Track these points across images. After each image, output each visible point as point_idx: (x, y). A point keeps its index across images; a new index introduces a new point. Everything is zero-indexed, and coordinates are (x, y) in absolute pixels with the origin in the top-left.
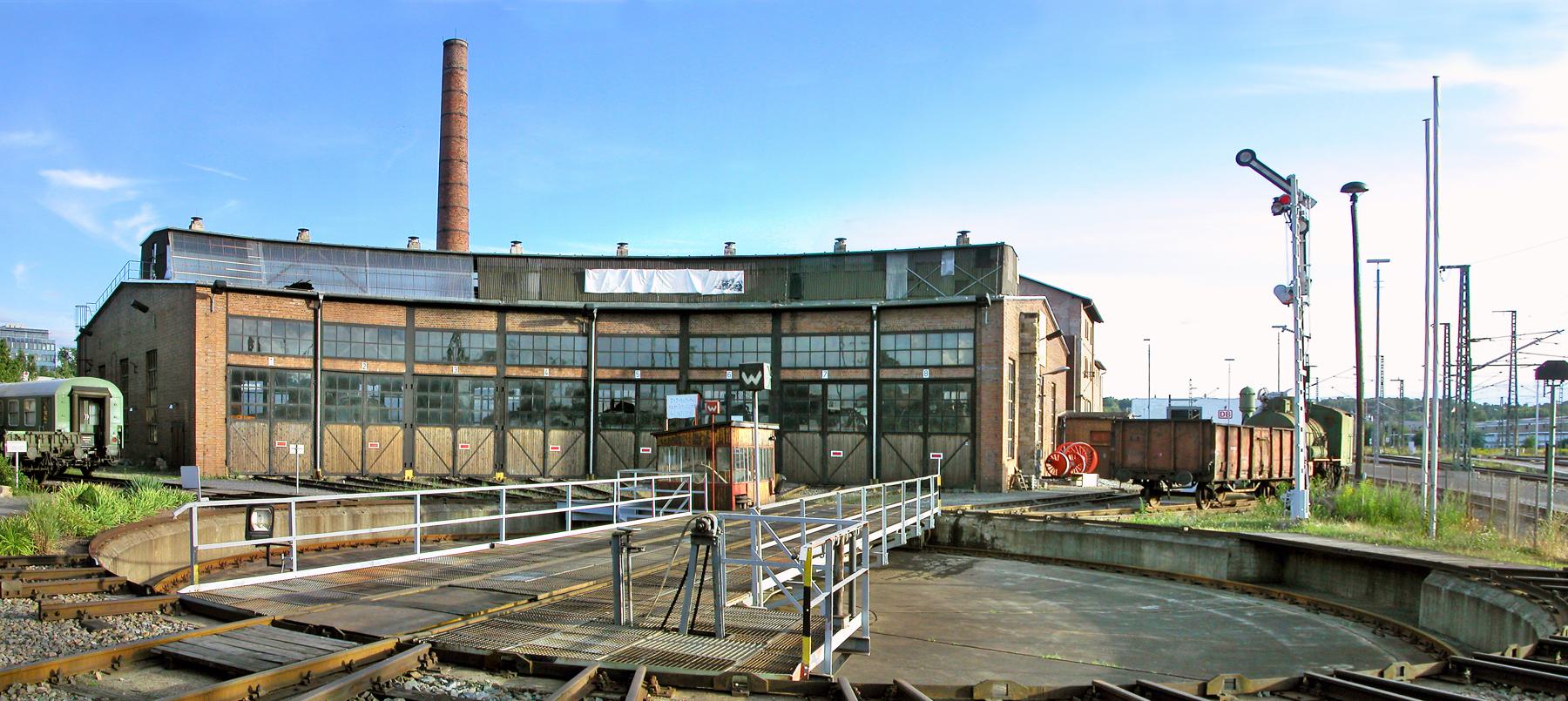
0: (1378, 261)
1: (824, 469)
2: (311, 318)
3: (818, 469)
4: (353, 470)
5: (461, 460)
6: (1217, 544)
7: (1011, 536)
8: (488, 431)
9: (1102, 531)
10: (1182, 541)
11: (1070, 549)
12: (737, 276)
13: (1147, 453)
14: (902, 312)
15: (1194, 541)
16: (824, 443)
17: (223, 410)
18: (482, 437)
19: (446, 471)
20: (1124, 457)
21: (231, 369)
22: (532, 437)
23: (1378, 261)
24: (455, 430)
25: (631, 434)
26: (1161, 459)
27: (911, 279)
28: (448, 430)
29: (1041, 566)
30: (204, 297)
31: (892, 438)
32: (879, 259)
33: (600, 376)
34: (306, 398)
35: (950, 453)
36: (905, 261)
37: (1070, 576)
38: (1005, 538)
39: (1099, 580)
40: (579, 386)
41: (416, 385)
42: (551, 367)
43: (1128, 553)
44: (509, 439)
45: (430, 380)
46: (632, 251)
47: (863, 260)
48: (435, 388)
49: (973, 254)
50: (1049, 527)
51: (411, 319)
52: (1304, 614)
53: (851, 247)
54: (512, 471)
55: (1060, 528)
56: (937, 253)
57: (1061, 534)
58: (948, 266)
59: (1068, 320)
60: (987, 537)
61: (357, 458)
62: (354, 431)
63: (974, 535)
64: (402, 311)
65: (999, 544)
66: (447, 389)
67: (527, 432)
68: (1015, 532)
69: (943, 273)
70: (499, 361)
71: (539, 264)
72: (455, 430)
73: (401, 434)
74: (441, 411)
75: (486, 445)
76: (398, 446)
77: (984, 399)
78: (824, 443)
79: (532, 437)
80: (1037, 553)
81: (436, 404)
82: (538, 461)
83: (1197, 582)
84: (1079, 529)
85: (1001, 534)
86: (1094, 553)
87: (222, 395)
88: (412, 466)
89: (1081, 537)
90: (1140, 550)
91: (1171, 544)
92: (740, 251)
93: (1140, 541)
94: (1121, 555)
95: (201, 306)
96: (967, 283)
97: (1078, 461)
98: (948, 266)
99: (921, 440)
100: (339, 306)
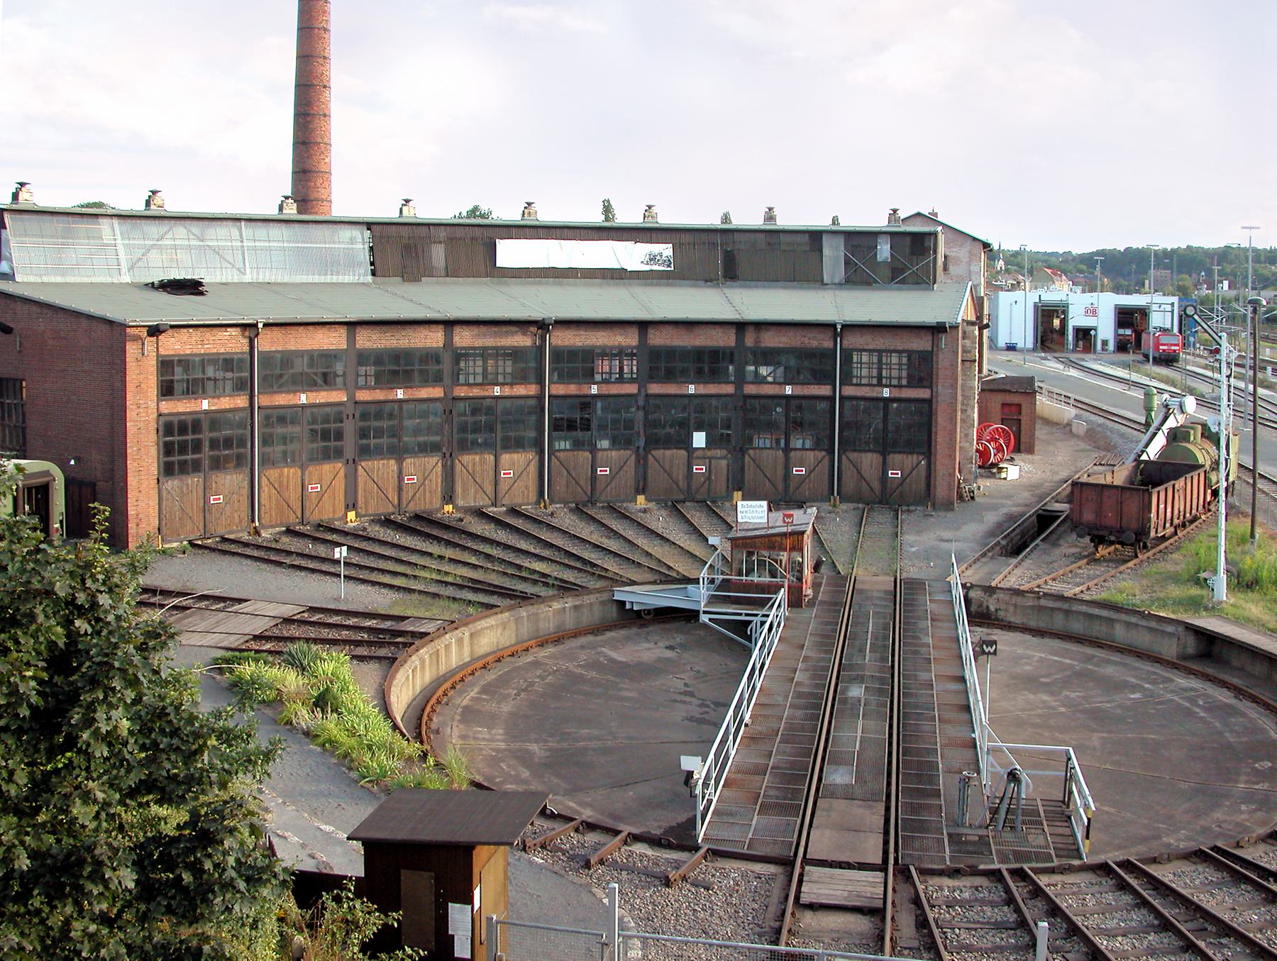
0: (1251, 228)
1: (787, 488)
2: (246, 349)
3: (781, 486)
4: (292, 519)
5: (408, 495)
6: (1170, 629)
7: (1011, 609)
8: (435, 459)
9: (1084, 608)
10: (1144, 623)
11: (1059, 622)
12: (666, 250)
13: (1099, 513)
14: (864, 330)
15: (1153, 624)
16: (787, 459)
17: (154, 469)
18: (429, 467)
19: (391, 509)
20: (1081, 513)
21: (162, 419)
22: (482, 462)
23: (1251, 228)
24: (400, 461)
25: (588, 455)
26: (1110, 518)
27: (848, 263)
28: (392, 462)
29: (1036, 640)
30: (137, 338)
31: (853, 456)
32: (815, 237)
33: (554, 392)
34: (242, 443)
35: (907, 471)
36: (840, 241)
37: (1065, 654)
38: (1006, 610)
39: (1090, 659)
40: (533, 402)
41: (357, 415)
42: (502, 385)
43: (1104, 628)
44: (458, 467)
45: (373, 409)
46: (546, 215)
47: (799, 238)
48: (379, 416)
49: (908, 239)
50: (1043, 602)
51: (351, 339)
52: (1233, 701)
53: (784, 221)
54: (461, 503)
55: (1050, 604)
56: (870, 236)
57: (1052, 609)
58: (884, 250)
59: (969, 263)
60: (992, 608)
61: (297, 506)
62: (291, 474)
63: (981, 605)
64: (343, 331)
65: (1001, 614)
66: (391, 416)
67: (477, 458)
68: (1015, 606)
69: (879, 258)
70: (447, 380)
71: (443, 233)
72: (400, 461)
73: (342, 473)
74: (384, 441)
75: (433, 476)
76: (340, 484)
77: (940, 420)
78: (787, 459)
79: (482, 462)
80: (1032, 624)
81: (379, 433)
82: (489, 489)
83: (1158, 660)
84: (1066, 606)
85: (1003, 606)
86: (1077, 626)
87: (153, 451)
88: (354, 507)
89: (1068, 612)
90: (1113, 627)
91: (1137, 625)
92: (665, 218)
93: (1112, 620)
94: (1098, 630)
95: (132, 349)
96: (902, 271)
97: (999, 449)
98: (884, 250)
99: (881, 458)
100: (276, 332)
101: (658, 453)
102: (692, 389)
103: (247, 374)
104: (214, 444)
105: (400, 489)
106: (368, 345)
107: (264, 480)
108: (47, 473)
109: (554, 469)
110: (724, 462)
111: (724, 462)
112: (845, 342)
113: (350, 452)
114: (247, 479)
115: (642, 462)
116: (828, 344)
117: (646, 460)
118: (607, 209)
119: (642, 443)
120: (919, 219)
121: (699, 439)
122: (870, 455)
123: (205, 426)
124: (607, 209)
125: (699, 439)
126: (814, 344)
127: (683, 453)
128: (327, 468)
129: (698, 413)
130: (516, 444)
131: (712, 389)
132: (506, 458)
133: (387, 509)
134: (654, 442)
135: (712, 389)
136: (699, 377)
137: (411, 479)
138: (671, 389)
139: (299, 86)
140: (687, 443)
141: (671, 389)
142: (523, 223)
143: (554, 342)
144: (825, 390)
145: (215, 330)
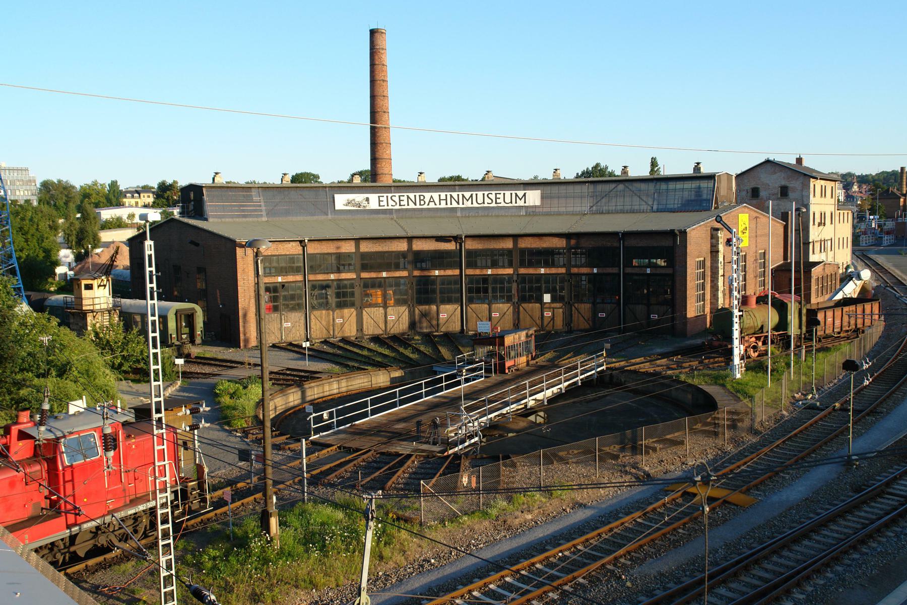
2: (301, 252)
8: (404, 308)
25: (486, 306)
34: (300, 297)
51: (357, 247)
59: (802, 191)
73: (355, 313)
75: (404, 316)
76: (354, 319)
95: (239, 252)
100: (316, 244)
101: (525, 305)
102: (543, 271)
103: (302, 265)
104: (285, 298)
105: (386, 322)
106: (366, 250)
107: (312, 317)
108: (193, 309)
109: (469, 314)
110: (561, 310)
111: (561, 310)
112: (626, 243)
113: (357, 303)
114: (304, 315)
115: (517, 313)
116: (616, 244)
117: (518, 309)
118: (654, 163)
119: (516, 300)
120: (768, 166)
121: (547, 298)
122: (640, 306)
123: (280, 289)
124: (654, 163)
125: (547, 298)
126: (609, 244)
127: (538, 305)
128: (346, 311)
129: (549, 284)
130: (449, 301)
131: (554, 271)
132: (442, 307)
133: (378, 332)
134: (523, 299)
135: (554, 271)
136: (547, 265)
137: (391, 318)
138: (531, 271)
139: (371, 113)
140: (540, 300)
141: (531, 271)
142: (652, 177)
143: (467, 247)
144: (614, 270)
145: (284, 243)
